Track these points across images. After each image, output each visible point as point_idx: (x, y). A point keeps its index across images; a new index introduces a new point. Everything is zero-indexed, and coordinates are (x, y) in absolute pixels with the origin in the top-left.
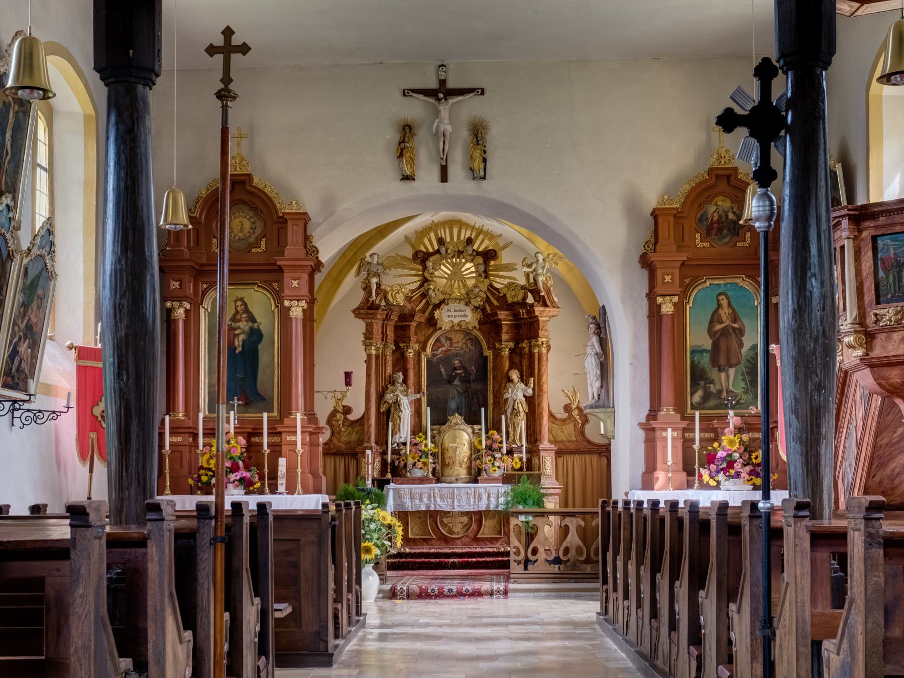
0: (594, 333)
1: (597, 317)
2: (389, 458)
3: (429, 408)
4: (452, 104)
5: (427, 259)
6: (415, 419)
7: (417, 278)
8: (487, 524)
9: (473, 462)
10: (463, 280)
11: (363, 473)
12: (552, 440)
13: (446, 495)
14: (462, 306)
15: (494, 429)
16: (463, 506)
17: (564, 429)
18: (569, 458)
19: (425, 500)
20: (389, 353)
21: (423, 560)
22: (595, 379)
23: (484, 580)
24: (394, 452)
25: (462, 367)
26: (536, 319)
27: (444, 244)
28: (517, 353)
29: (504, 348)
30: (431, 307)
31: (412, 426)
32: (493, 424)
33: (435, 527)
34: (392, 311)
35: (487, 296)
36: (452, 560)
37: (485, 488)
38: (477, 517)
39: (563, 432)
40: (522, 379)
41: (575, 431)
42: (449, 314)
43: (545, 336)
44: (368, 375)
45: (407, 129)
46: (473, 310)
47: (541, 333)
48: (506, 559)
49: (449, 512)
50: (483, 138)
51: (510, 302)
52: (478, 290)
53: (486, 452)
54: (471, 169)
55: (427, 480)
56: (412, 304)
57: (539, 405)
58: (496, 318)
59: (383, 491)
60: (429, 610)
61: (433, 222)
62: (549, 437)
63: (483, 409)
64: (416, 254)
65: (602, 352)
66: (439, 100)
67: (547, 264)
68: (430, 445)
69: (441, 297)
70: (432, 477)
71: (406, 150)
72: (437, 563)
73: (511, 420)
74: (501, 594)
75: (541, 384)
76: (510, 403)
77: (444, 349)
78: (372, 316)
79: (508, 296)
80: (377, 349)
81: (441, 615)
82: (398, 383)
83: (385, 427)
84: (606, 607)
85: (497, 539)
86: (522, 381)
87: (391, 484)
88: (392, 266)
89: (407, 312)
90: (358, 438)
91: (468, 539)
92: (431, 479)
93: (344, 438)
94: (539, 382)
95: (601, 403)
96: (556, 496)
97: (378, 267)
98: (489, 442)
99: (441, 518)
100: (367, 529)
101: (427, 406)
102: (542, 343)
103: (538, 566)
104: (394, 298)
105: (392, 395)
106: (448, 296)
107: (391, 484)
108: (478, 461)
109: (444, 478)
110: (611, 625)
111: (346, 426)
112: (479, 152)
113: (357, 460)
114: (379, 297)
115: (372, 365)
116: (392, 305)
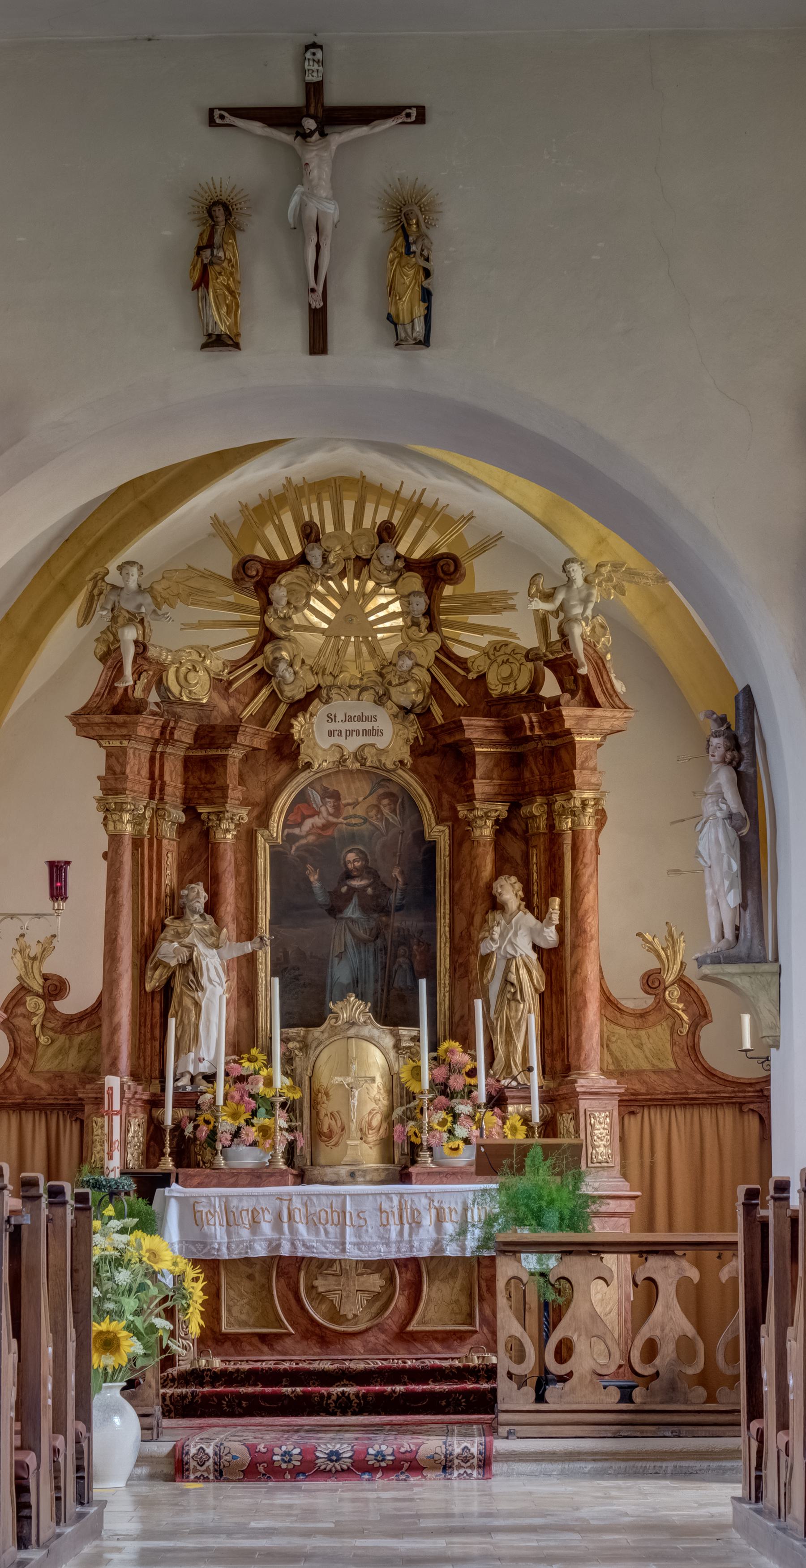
0: (723, 761)
1: (731, 719)
2: (168, 1116)
3: (276, 981)
4: (341, 147)
5: (273, 580)
6: (238, 1010)
7: (243, 632)
8: (433, 1294)
9: (398, 1127)
10: (367, 632)
11: (96, 1157)
12: (611, 1067)
13: (323, 1214)
14: (367, 705)
15: (454, 1038)
16: (369, 1245)
17: (644, 1039)
18: (657, 1118)
19: (266, 1228)
20: (168, 831)
21: (259, 1389)
22: (727, 883)
23: (427, 1433)
24: (183, 1100)
25: (369, 871)
26: (566, 739)
27: (318, 540)
28: (515, 833)
29: (481, 818)
30: (282, 709)
31: (232, 1030)
32: (451, 1023)
33: (293, 1302)
34: (178, 718)
35: (433, 678)
36: (341, 1389)
37: (430, 1196)
38: (409, 1276)
39: (640, 1046)
40: (528, 903)
41: (673, 1044)
42: (333, 726)
43: (590, 784)
44: (113, 891)
45: (219, 212)
46: (395, 716)
47: (579, 776)
48: (486, 1386)
49: (331, 1262)
50: (421, 236)
51: (495, 694)
52: (408, 663)
53: (431, 1101)
54: (389, 317)
55: (272, 1175)
56: (233, 702)
57: (575, 972)
58: (458, 737)
59: (150, 1203)
60: (278, 1502)
61: (289, 480)
62: (602, 1061)
63: (423, 983)
64: (243, 566)
65: (744, 813)
66: (305, 136)
67: (595, 592)
68: (280, 1081)
69: (311, 681)
70: (284, 1167)
71: (217, 268)
72: (298, 1396)
73: (499, 1011)
74: (471, 1467)
75: (580, 914)
76: (497, 965)
77: (318, 821)
78: (124, 731)
79: (492, 680)
80: (137, 821)
81: (309, 1513)
82: (194, 912)
83: (157, 1032)
84: (759, 1478)
85: (461, 1337)
86: (529, 907)
87: (174, 1186)
88: (178, 595)
89: (217, 719)
90: (82, 1063)
91: (383, 1337)
92: (282, 1173)
93: (46, 1064)
94: (575, 909)
95: (742, 948)
96: (623, 1220)
97: (140, 599)
98: (441, 1072)
99: (310, 1277)
100: (108, 1285)
101: (273, 974)
102: (584, 803)
103: (573, 1390)
104: (185, 682)
105: (176, 944)
106: (329, 680)
107: (174, 1186)
108: (411, 1123)
109: (316, 1171)
110: (771, 1519)
111: (52, 1029)
112: (411, 272)
113: (82, 1122)
114: (144, 680)
115: (121, 862)
116: (179, 701)
